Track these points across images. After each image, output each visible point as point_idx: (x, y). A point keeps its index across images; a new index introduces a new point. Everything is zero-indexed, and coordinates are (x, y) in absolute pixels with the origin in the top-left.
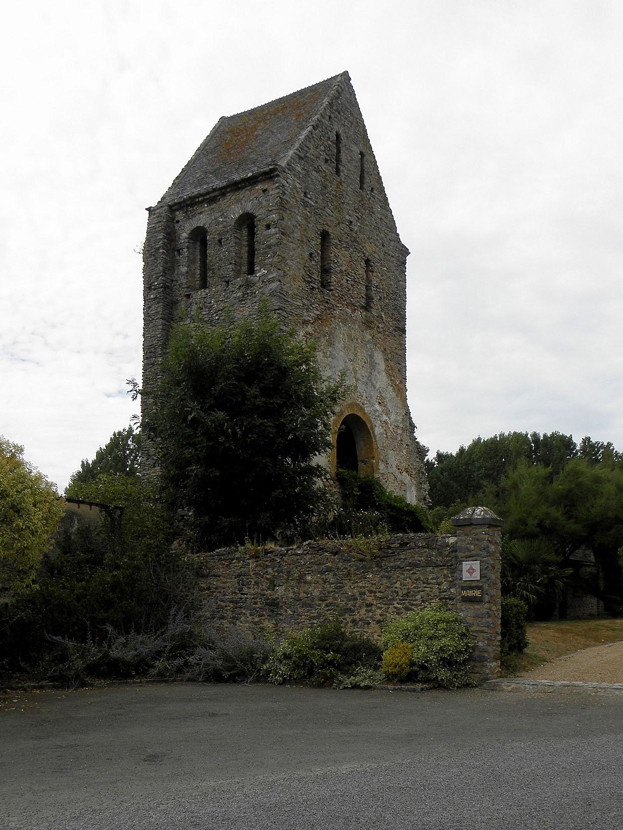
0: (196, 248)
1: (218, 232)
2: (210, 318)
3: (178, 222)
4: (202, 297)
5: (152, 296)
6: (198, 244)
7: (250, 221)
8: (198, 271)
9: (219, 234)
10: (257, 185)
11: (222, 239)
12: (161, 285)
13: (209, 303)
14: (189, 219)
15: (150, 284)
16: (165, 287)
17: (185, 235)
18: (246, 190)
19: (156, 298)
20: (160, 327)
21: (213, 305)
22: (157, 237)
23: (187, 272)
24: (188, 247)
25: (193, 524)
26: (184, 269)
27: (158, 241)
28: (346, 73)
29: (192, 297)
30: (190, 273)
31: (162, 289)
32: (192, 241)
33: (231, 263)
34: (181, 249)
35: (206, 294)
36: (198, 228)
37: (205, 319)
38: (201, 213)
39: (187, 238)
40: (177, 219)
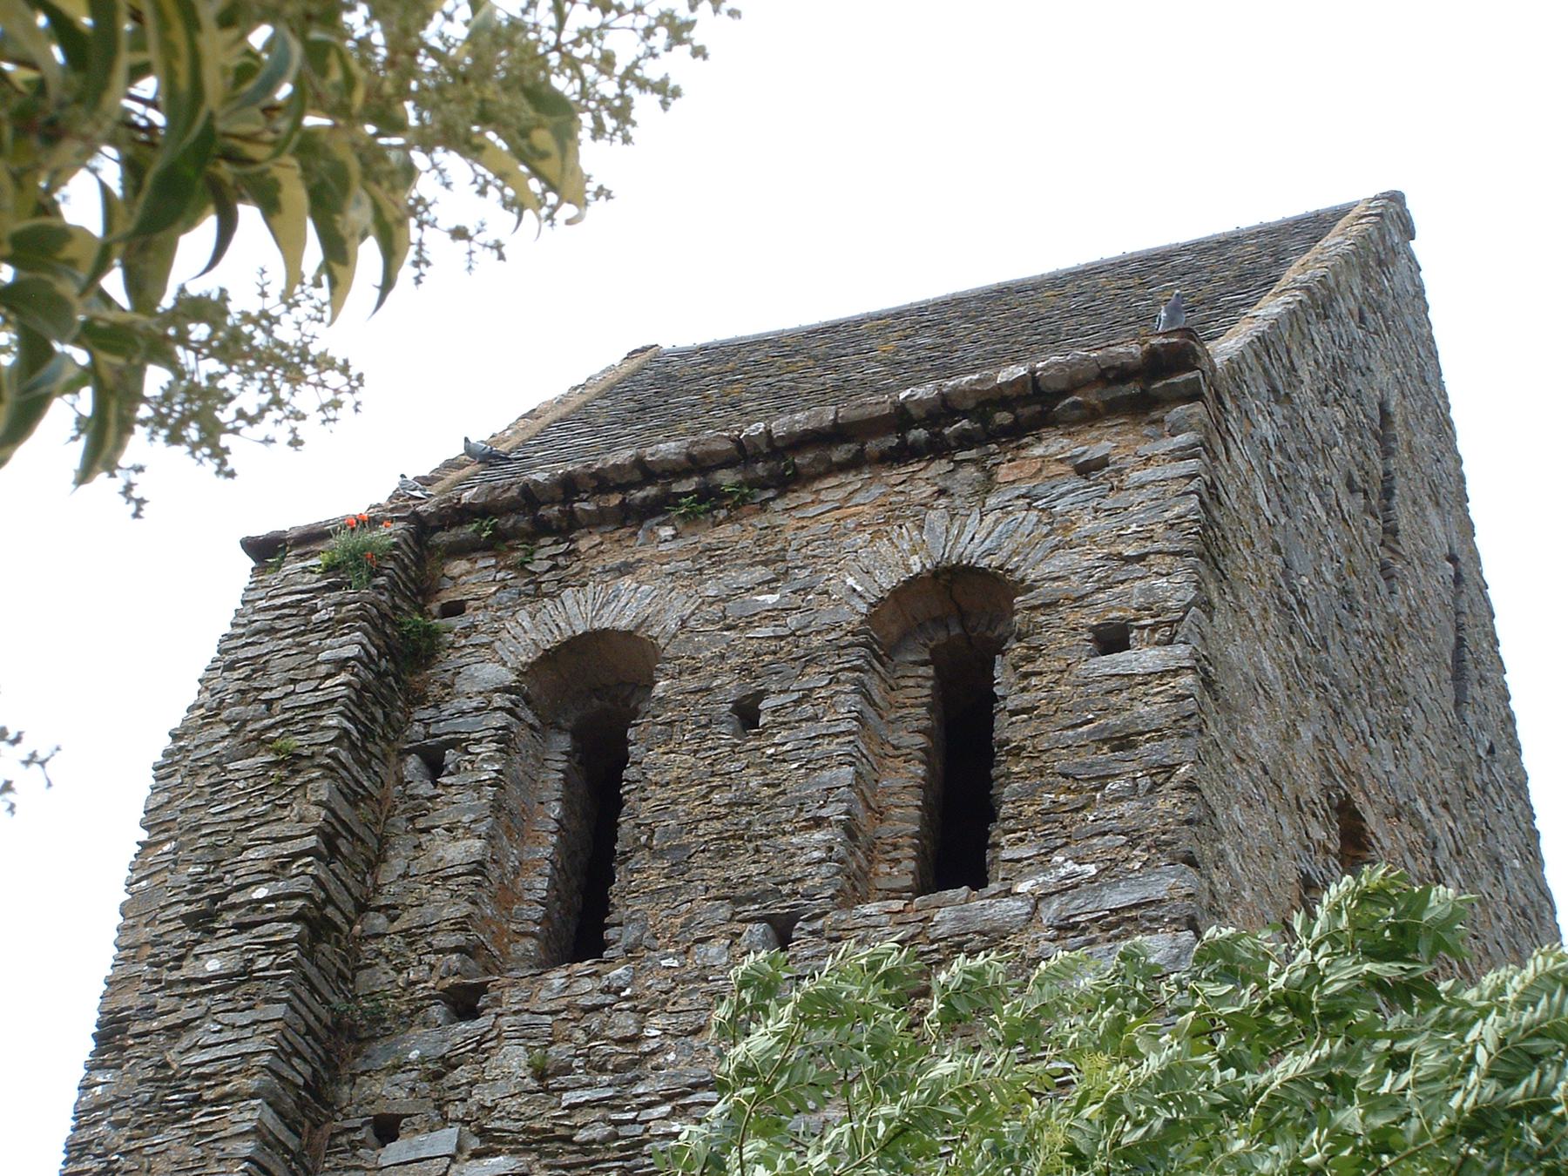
0: (542, 763)
1: (735, 661)
2: (623, 1131)
3: (456, 609)
4: (567, 1008)
5: (213, 965)
6: (564, 742)
7: (956, 630)
8: (541, 884)
9: (745, 670)
10: (1040, 439)
11: (761, 695)
12: (299, 903)
13: (623, 1041)
14: (538, 595)
15: (214, 899)
16: (317, 926)
17: (491, 673)
18: (959, 463)
19: (246, 973)
20: (246, 1147)
21: (653, 1052)
22: (318, 650)
23: (479, 868)
24: (504, 739)
25: (207, 343)
26: (458, 851)
27: (322, 670)
28: (1396, 198)
29: (497, 1001)
30: (494, 873)
31: (297, 928)
32: (528, 715)
33: (818, 823)
34: (452, 744)
35: (606, 991)
36: (597, 639)
37: (582, 1136)
38: (624, 569)
39: (507, 690)
40: (450, 595)
